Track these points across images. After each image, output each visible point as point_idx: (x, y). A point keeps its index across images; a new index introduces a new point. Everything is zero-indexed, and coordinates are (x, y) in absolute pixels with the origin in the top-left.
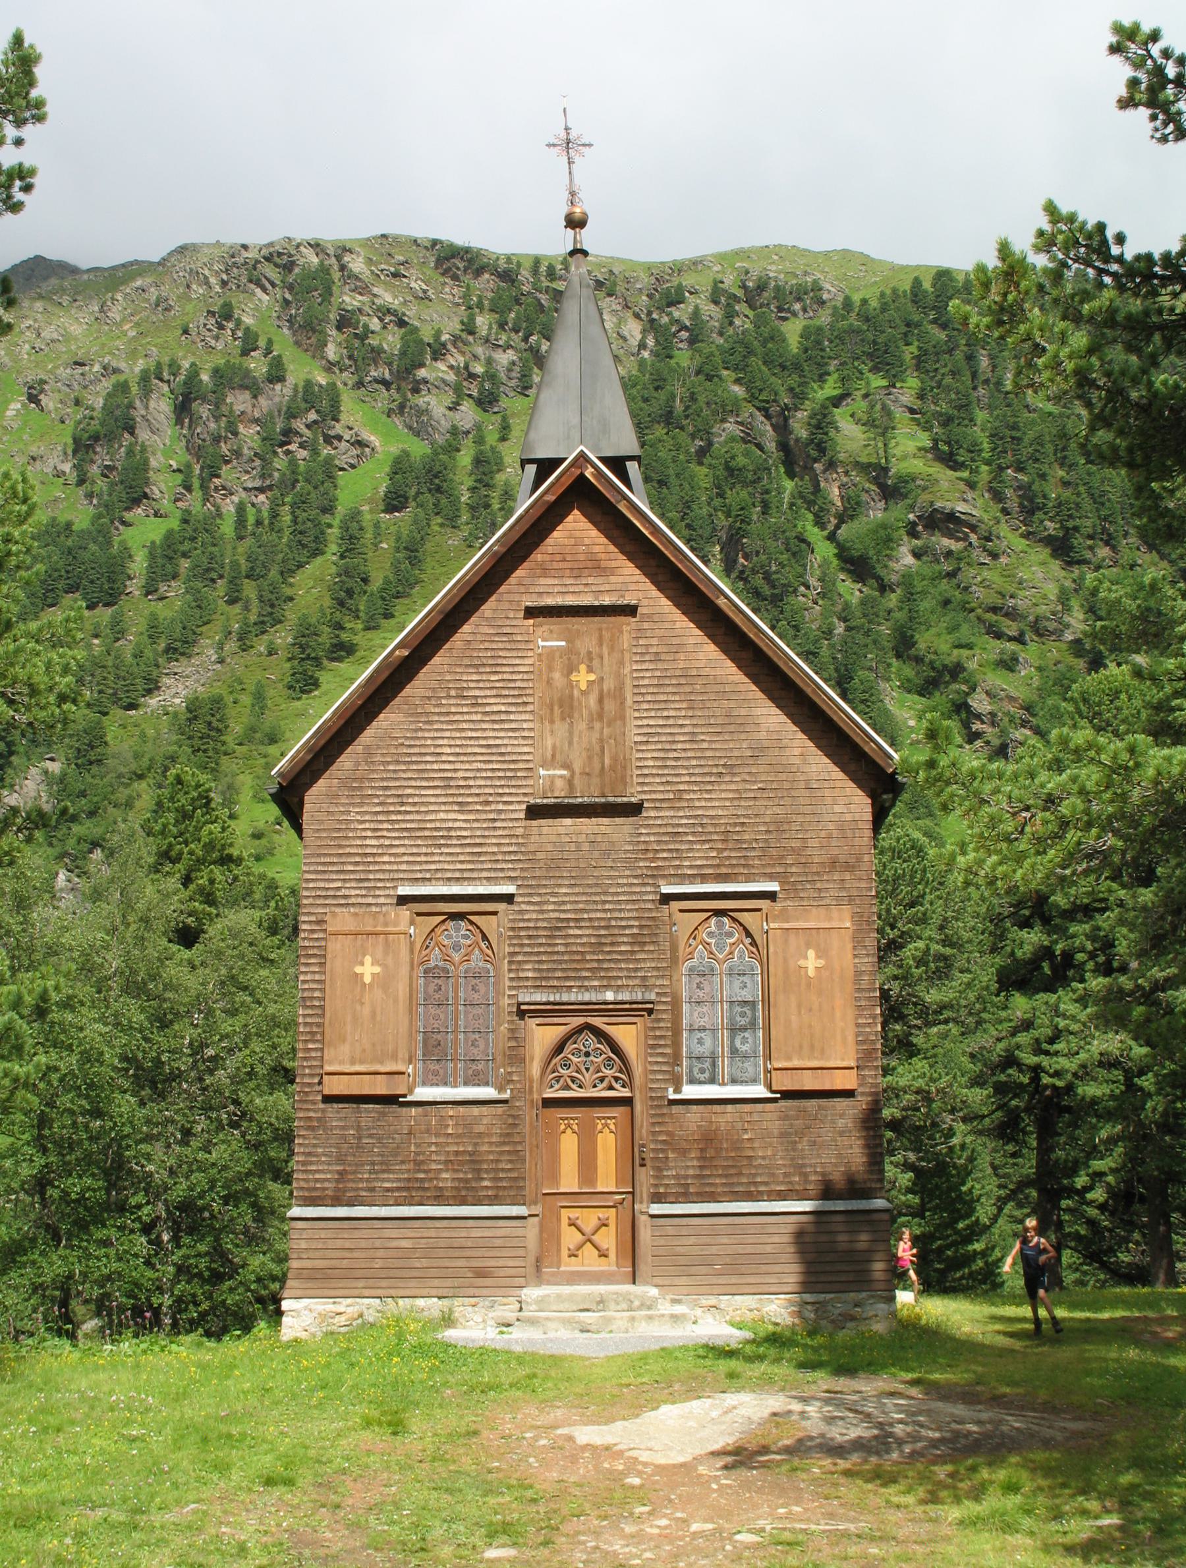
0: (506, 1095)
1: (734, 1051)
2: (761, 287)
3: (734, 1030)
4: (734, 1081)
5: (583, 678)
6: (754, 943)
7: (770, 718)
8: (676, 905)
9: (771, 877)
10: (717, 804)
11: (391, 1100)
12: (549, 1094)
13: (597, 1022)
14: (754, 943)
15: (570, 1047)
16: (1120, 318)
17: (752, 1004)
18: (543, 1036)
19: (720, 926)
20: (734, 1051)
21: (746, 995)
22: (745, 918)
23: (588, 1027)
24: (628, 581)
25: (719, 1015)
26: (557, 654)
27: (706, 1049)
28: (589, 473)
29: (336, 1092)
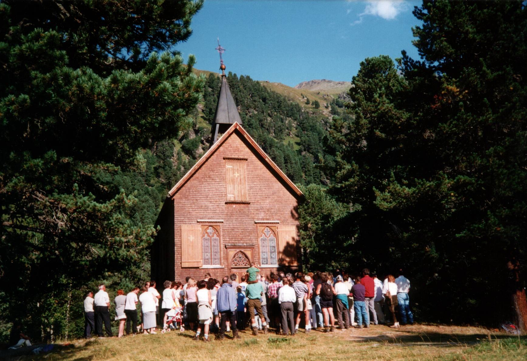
0: (223, 267)
1: (271, 257)
2: (272, 274)
3: (271, 253)
4: (271, 264)
5: (237, 175)
6: (275, 234)
7: (279, 185)
8: (258, 225)
9: (278, 219)
10: (267, 204)
11: (198, 268)
12: (232, 266)
13: (242, 250)
14: (275, 234)
15: (236, 256)
16: (244, 278)
17: (274, 247)
18: (232, 253)
19: (267, 229)
20: (271, 257)
21: (273, 245)
22: (273, 228)
23: (241, 251)
24: (246, 152)
25: (267, 249)
26: (323, 302)
27: (265, 257)
28: (238, 128)
29: (185, 266)
